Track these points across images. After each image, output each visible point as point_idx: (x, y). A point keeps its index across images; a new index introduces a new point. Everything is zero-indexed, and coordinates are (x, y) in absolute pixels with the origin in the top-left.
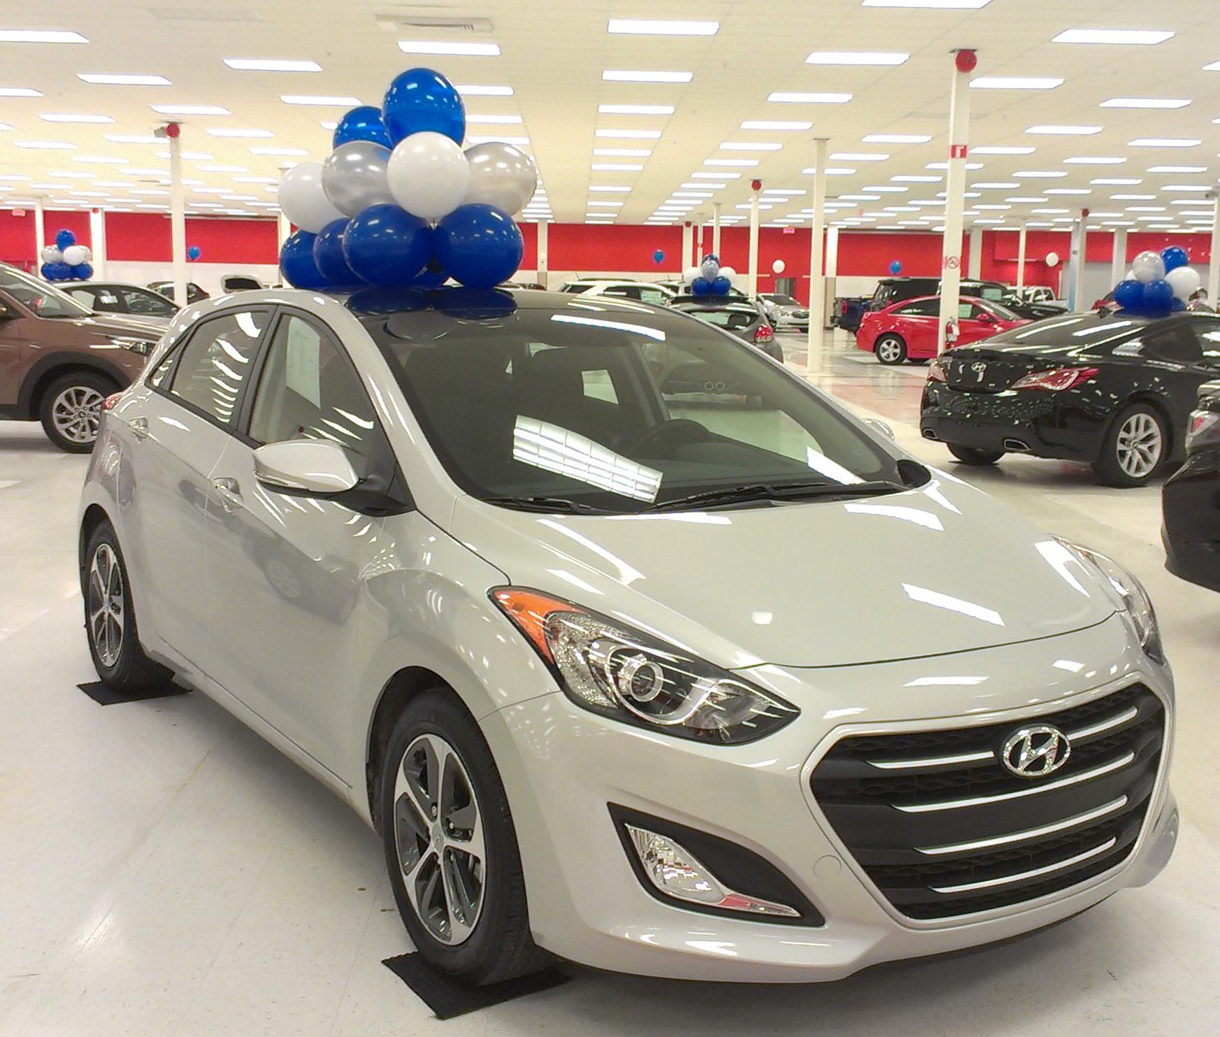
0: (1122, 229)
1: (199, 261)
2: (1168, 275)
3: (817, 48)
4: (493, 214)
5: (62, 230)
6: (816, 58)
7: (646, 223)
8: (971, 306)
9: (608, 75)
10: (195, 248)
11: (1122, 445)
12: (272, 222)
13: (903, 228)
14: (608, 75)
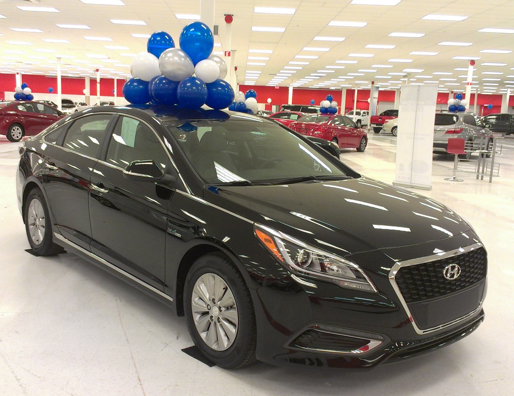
0: (398, 90)
1: (53, 93)
2: (247, 100)
3: (333, 19)
4: (221, 82)
5: (25, 83)
6: (333, 23)
7: (266, 85)
8: (297, 115)
9: (254, 29)
10: (51, 88)
11: (316, 164)
12: (55, 78)
13: (319, 87)
14: (254, 29)
